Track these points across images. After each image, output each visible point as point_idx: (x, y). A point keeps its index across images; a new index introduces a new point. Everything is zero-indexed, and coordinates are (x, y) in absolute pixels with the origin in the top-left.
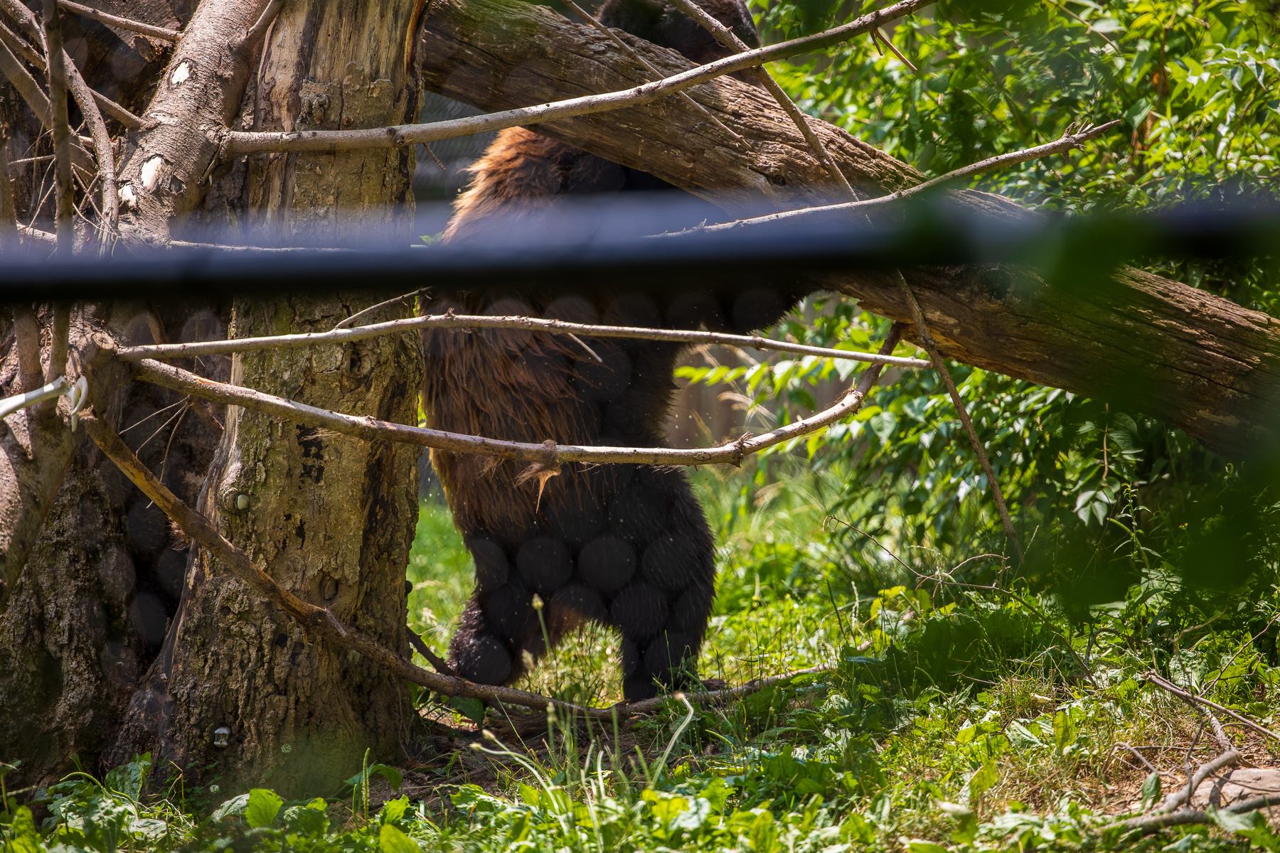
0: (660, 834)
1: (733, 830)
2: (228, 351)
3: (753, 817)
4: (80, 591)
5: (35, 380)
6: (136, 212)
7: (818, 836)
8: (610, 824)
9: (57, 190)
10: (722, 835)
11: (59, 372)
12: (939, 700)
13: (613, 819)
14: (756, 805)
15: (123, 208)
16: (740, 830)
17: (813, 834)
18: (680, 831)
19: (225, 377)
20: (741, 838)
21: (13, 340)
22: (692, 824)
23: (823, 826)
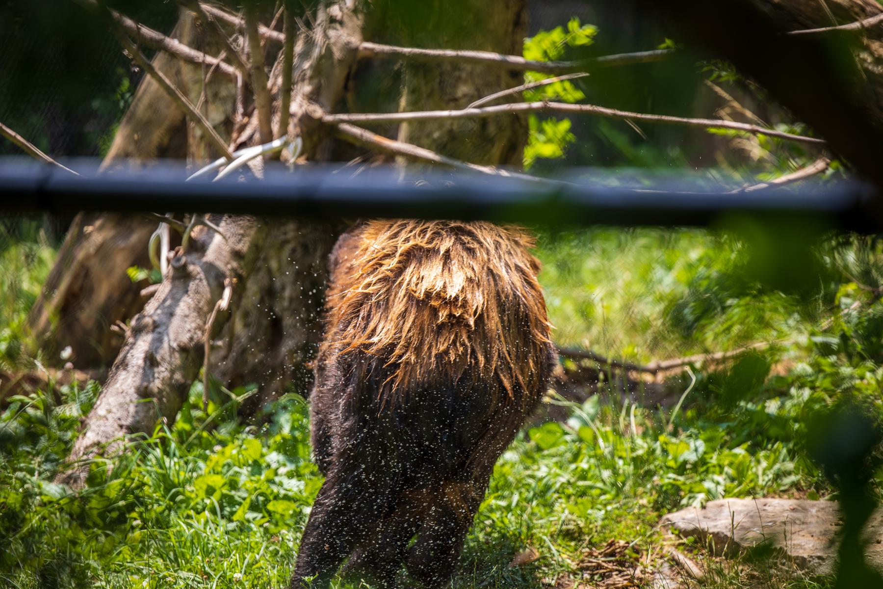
0: (671, 464)
1: (721, 463)
2: (401, 121)
3: (736, 455)
4: (298, 274)
5: (267, 137)
6: (341, 23)
7: (779, 469)
8: (638, 456)
9: (285, 13)
10: (714, 466)
11: (284, 132)
12: (873, 371)
13: (640, 452)
14: (738, 445)
15: (332, 20)
16: (727, 462)
17: (777, 466)
18: (685, 462)
19: (394, 137)
20: (726, 469)
21: (254, 109)
22: (692, 457)
23: (784, 461)
